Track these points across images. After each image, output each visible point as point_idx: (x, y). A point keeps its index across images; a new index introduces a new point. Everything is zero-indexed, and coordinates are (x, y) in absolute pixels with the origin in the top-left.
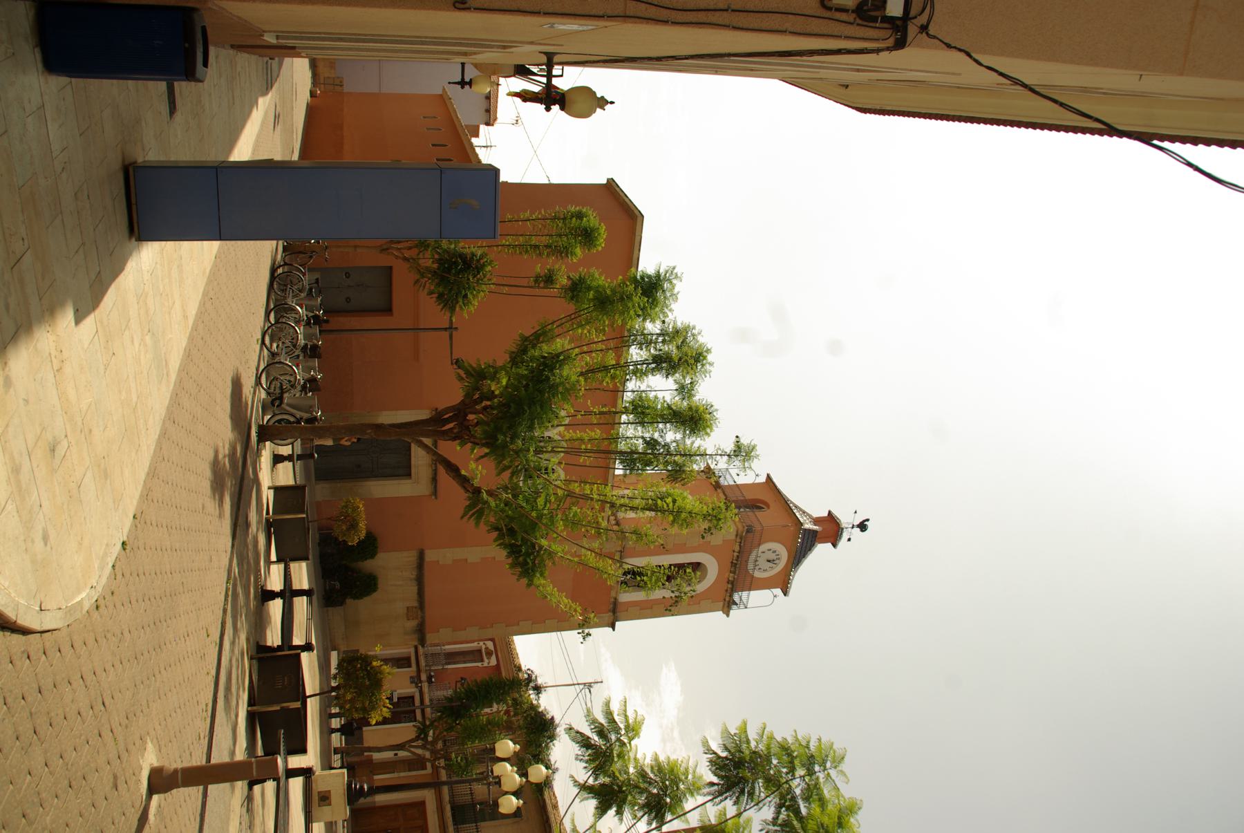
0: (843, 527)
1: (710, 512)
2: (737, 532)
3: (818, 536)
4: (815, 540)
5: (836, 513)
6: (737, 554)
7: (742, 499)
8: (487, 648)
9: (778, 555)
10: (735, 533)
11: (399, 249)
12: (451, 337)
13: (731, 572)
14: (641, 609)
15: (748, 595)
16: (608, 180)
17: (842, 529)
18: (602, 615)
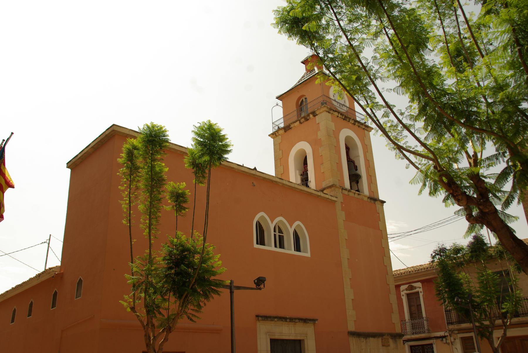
2: (327, 111)
8: (407, 290)
10: (328, 113)
11: (154, 337)
12: (238, 288)
13: (349, 121)
16: (68, 167)
18: (377, 208)
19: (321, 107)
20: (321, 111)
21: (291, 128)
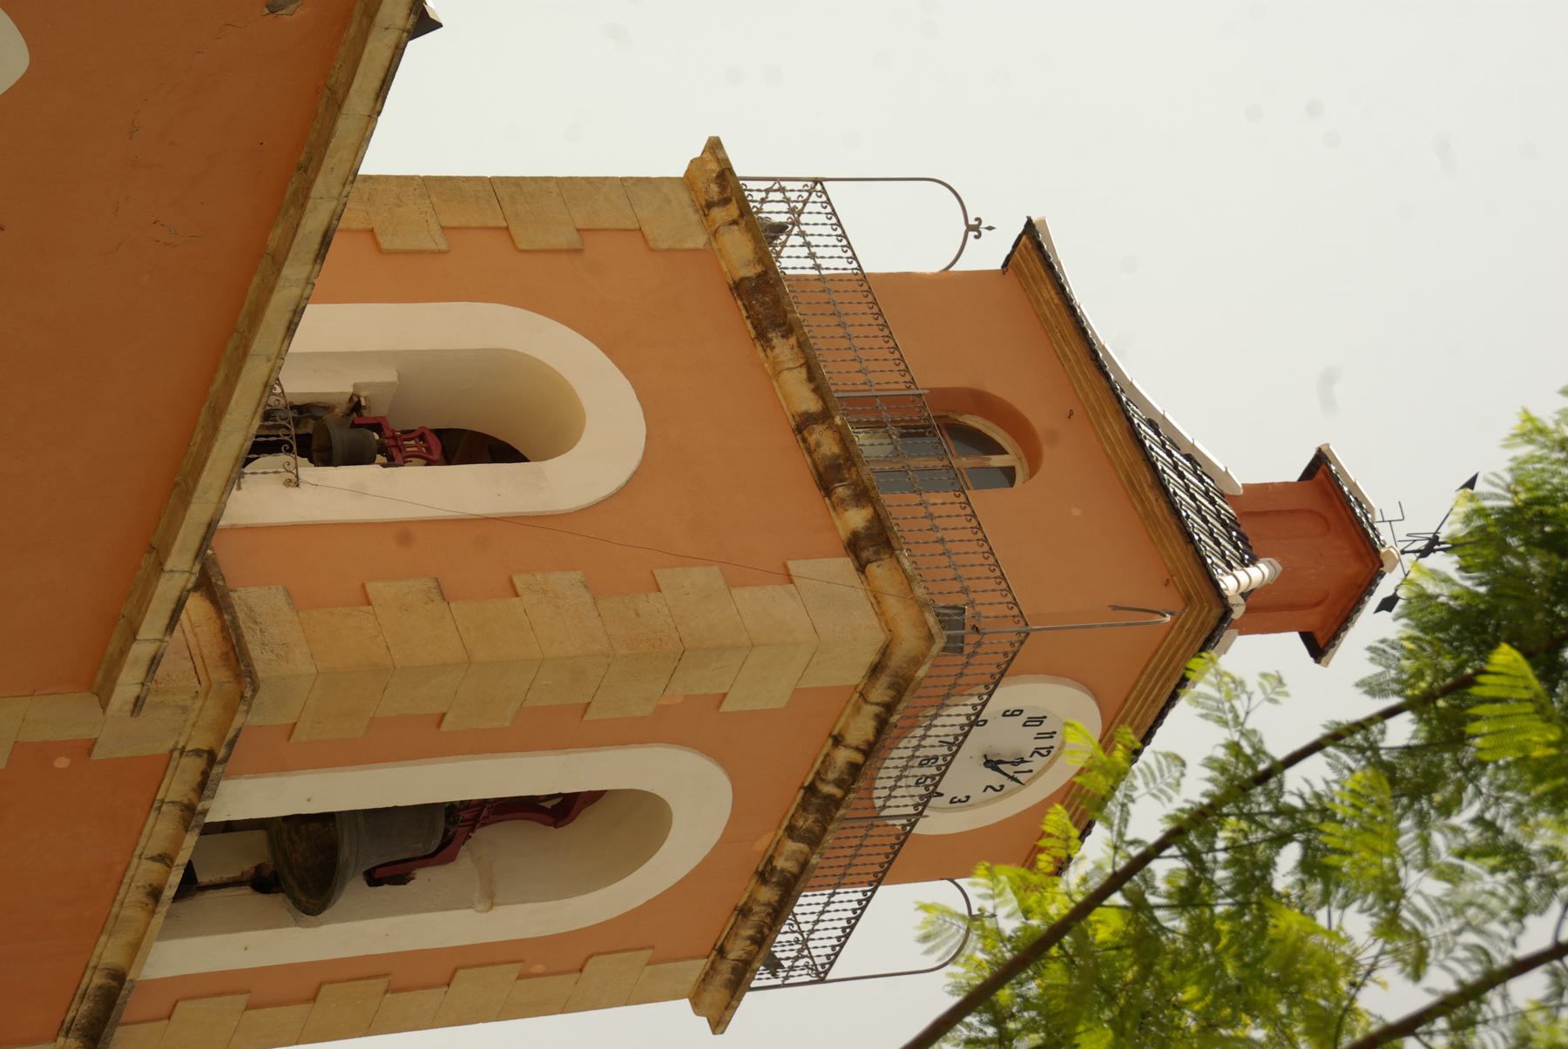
2: (885, 652)
5: (1354, 467)
6: (858, 758)
9: (1051, 735)
10: (869, 657)
13: (791, 831)
14: (250, 1007)
20: (893, 605)
21: (762, 336)
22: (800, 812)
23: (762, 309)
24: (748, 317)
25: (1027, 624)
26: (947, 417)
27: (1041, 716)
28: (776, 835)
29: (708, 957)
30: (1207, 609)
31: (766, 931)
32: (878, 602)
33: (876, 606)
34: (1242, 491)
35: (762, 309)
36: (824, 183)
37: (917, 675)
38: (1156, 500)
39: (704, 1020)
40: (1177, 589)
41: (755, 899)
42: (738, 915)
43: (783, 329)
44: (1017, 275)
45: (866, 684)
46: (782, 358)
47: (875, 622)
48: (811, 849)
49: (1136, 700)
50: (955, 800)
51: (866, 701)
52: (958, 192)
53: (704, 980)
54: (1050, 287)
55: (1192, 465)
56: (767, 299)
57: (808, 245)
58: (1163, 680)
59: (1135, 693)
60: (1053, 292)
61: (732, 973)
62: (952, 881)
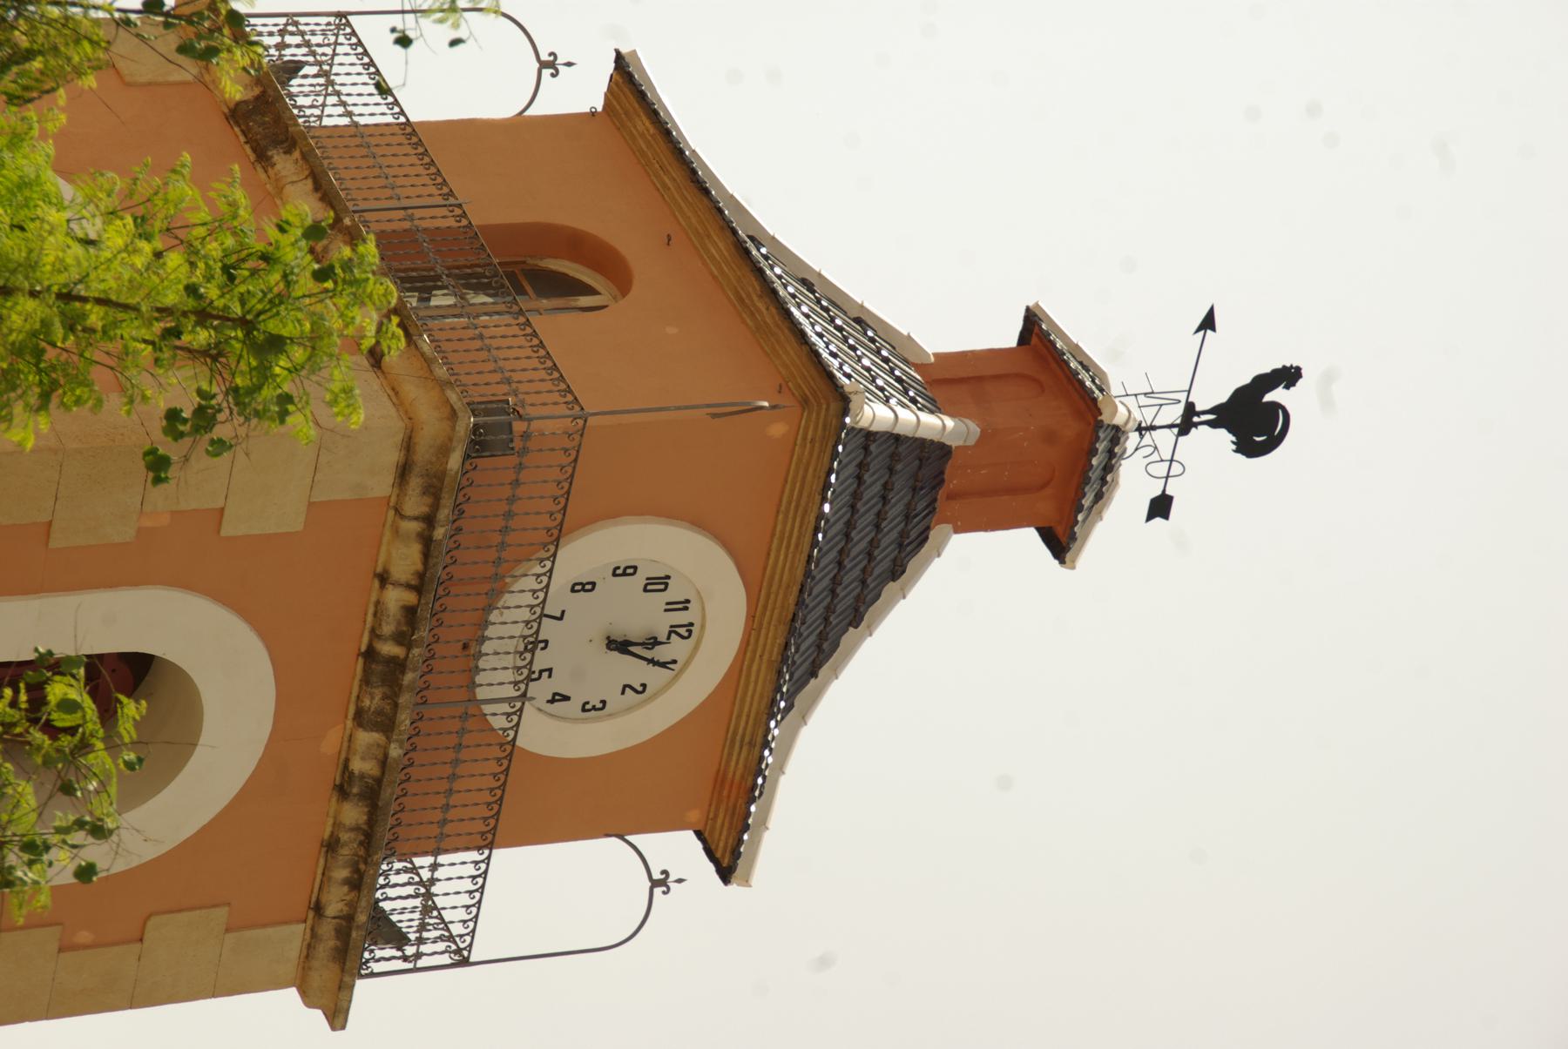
0: (1119, 420)
1: (212, 292)
2: (408, 445)
3: (952, 482)
4: (931, 508)
6: (410, 598)
7: (445, 221)
9: (685, 605)
10: (391, 457)
13: (360, 718)
15: (481, 876)
17: (1117, 434)
19: (443, 385)
20: (413, 391)
21: (262, 157)
22: (364, 688)
23: (261, 129)
24: (246, 143)
25: (582, 409)
26: (524, 262)
27: (663, 575)
28: (345, 729)
29: (305, 921)
30: (824, 406)
31: (362, 867)
32: (397, 393)
33: (394, 399)
34: (932, 359)
35: (261, 129)
36: (349, 17)
37: (449, 466)
38: (767, 309)
39: (318, 1014)
40: (793, 394)
41: (340, 823)
42: (327, 852)
43: (285, 145)
44: (609, 115)
45: (398, 496)
46: (284, 173)
47: (393, 411)
48: (387, 738)
49: (778, 551)
50: (588, 707)
51: (402, 517)
52: (525, 25)
53: (307, 957)
54: (644, 118)
55: (861, 327)
56: (267, 119)
57: (344, 104)
58: (800, 513)
59: (776, 541)
60: (647, 123)
61: (338, 938)
62: (621, 837)
